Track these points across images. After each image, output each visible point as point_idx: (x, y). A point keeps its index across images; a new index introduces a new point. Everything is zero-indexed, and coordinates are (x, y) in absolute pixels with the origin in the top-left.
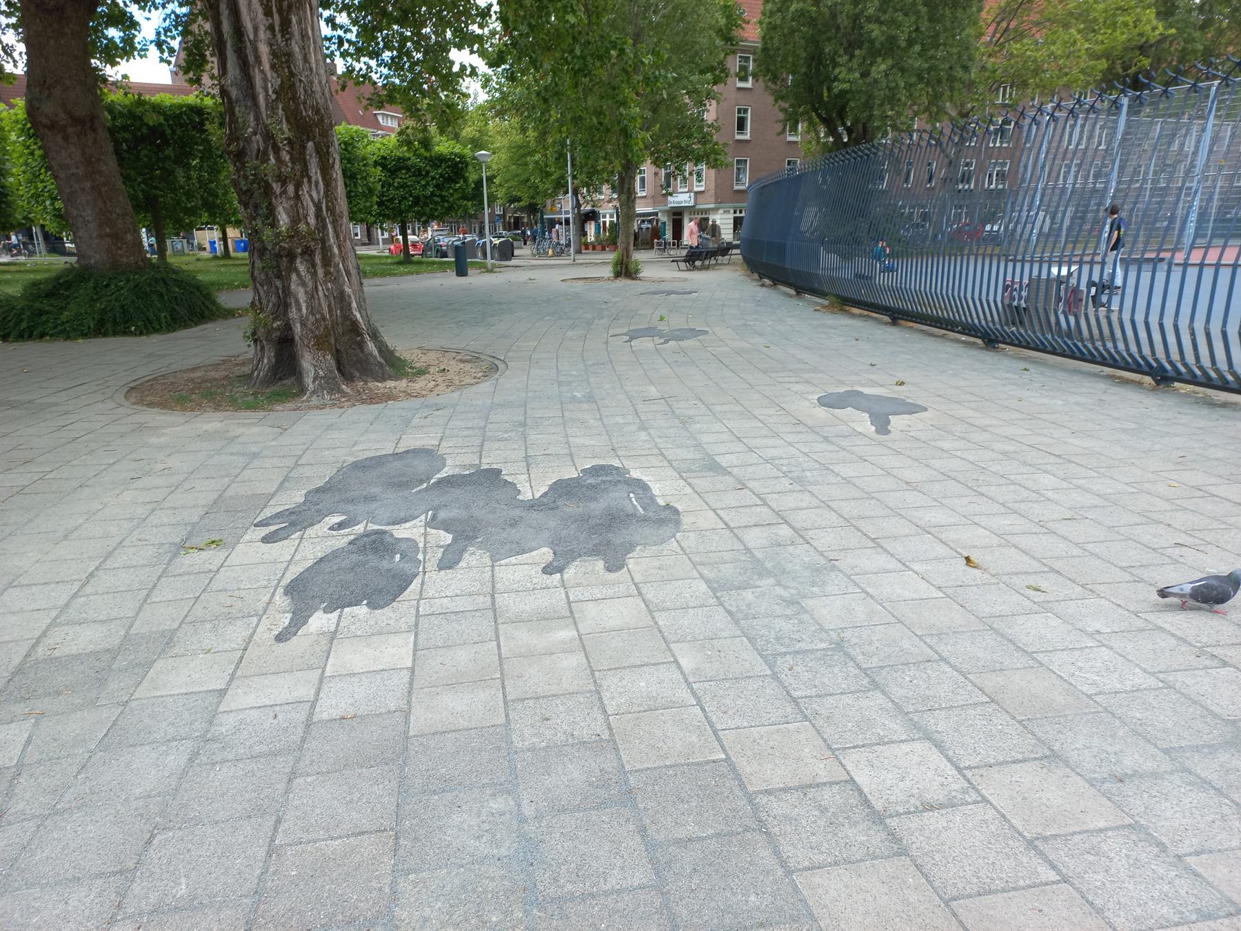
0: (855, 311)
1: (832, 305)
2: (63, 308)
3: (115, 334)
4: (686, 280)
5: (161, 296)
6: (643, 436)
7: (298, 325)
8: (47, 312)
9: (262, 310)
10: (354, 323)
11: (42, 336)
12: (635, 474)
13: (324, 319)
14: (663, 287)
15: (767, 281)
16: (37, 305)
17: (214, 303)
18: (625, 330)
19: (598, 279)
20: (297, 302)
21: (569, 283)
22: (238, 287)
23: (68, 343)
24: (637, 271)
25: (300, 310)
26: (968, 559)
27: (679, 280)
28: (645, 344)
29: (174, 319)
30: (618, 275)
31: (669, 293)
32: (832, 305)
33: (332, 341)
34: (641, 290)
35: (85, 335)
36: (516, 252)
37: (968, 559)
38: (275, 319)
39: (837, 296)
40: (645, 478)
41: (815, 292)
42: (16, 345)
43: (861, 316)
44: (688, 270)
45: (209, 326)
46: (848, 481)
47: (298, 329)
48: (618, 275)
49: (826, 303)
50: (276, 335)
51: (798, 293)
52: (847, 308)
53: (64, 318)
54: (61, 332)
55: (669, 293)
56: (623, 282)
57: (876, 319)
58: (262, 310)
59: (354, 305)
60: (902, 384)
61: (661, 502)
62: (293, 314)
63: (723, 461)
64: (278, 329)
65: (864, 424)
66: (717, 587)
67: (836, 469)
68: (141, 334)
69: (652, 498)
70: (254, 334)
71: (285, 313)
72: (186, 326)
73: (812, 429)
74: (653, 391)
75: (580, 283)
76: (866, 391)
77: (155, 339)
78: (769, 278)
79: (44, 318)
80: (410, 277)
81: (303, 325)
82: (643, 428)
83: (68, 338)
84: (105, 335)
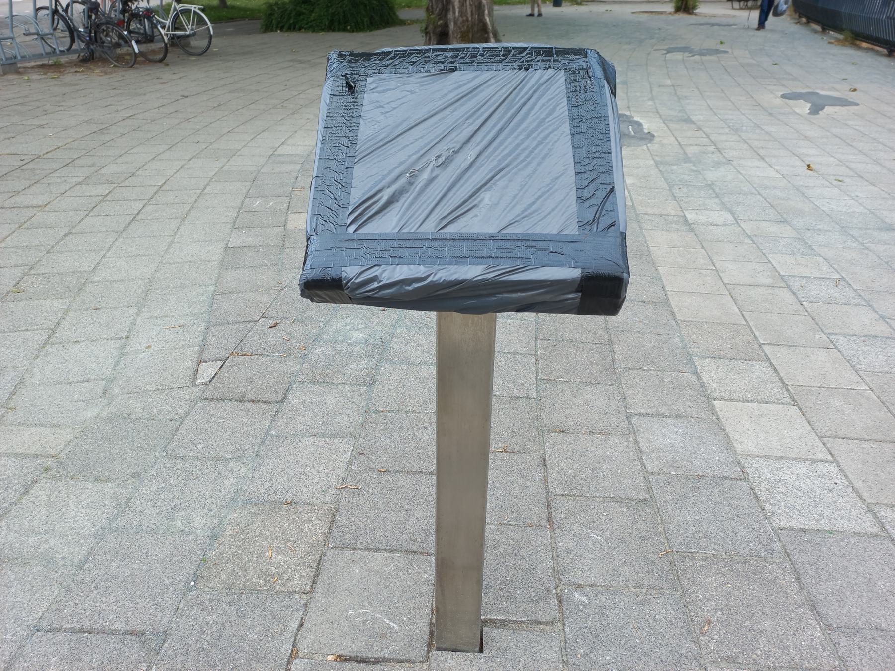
0: (864, 45)
1: (846, 40)
2: (312, 12)
3: (339, 30)
4: (734, 17)
5: (366, 6)
6: (650, 103)
7: (452, 24)
8: (303, 14)
9: (432, 13)
10: (485, 25)
11: (300, 29)
12: (636, 119)
13: (467, 20)
14: (713, 21)
15: (804, 20)
16: (298, 8)
17: (395, 14)
18: (666, 47)
19: (661, 13)
20: (454, 8)
21: (637, 15)
22: (404, 7)
23: (314, 34)
24: (694, 8)
25: (454, 13)
26: (809, 166)
27: (729, 16)
28: (678, 56)
29: (372, 23)
30: (678, 10)
31: (713, 25)
32: (846, 40)
33: (471, 36)
34: (692, 22)
35: (323, 30)
36: (621, 230)
37: (809, 166)
38: (440, 19)
39: (852, 32)
40: (641, 121)
41: (838, 29)
42: (286, 34)
43: (867, 49)
44: (741, 9)
45: (392, 29)
46: (767, 133)
47: (452, 26)
48: (678, 10)
49: (841, 37)
50: (439, 30)
51: (824, 30)
52: (858, 42)
53: (312, 18)
54: (311, 27)
55: (713, 25)
56: (682, 16)
57: (877, 51)
58: (432, 13)
59: (486, 12)
60: (855, 90)
61: (646, 131)
62: (450, 16)
63: (694, 118)
64: (440, 26)
65: (804, 108)
66: (657, 163)
67: (764, 127)
68: (353, 31)
69: (642, 129)
70: (426, 29)
71: (446, 15)
72: (378, 28)
73: (765, 110)
74: (668, 82)
75: (646, 15)
76: (822, 93)
77: (361, 34)
78: (806, 17)
79: (302, 17)
80: (519, 6)
81: (455, 23)
82: (652, 99)
83: (313, 31)
84: (333, 31)
